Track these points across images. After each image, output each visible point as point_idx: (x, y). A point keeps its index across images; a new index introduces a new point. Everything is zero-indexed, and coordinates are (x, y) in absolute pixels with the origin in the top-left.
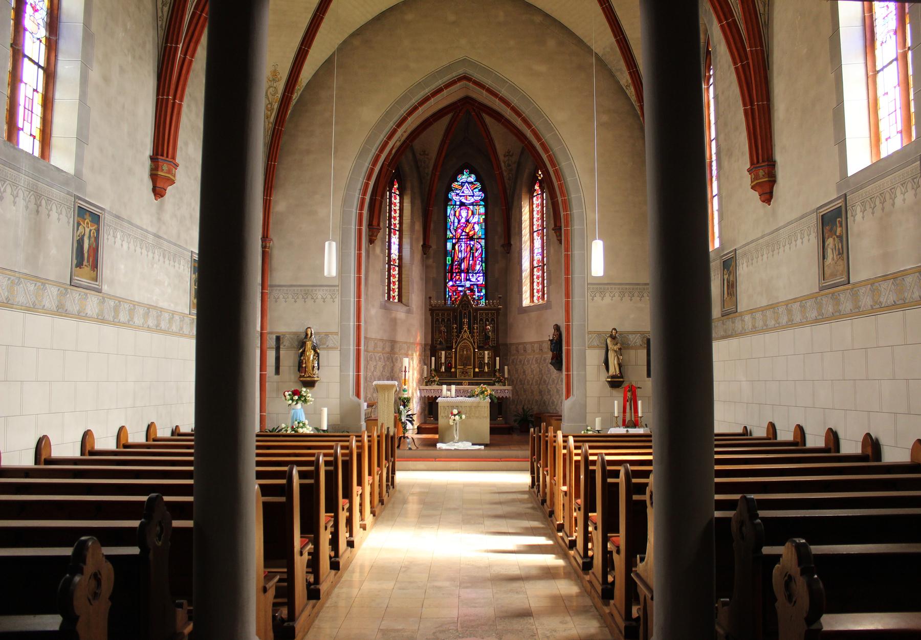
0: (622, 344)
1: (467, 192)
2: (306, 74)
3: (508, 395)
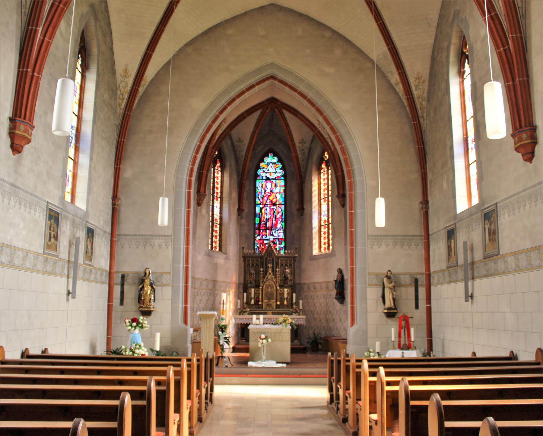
0: (395, 282)
3: (302, 322)
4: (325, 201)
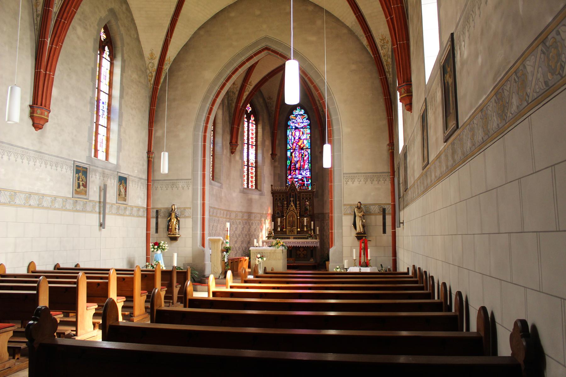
1: (299, 121)
2: (172, 54)
4: (252, 148)
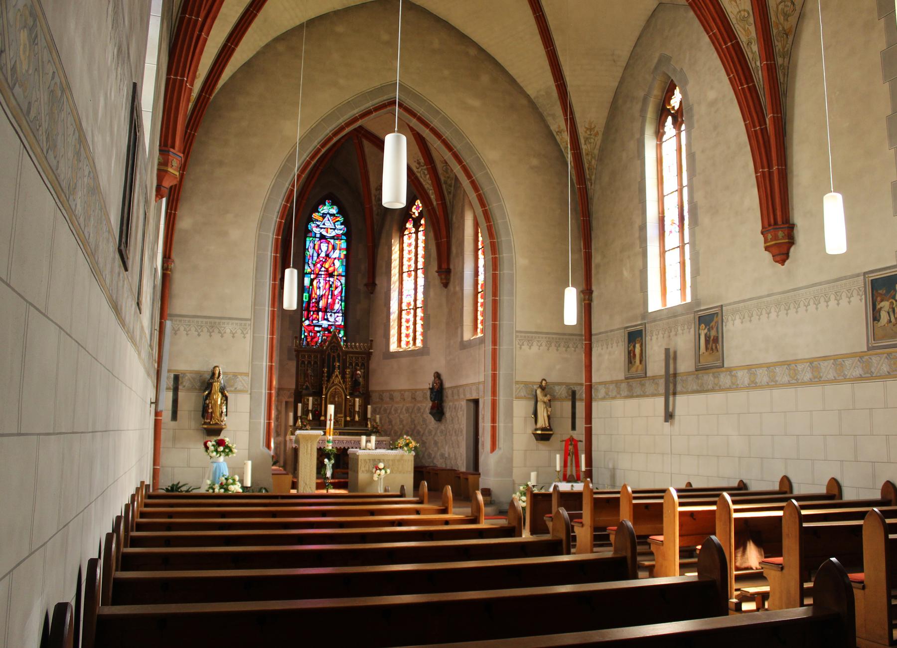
4: (409, 276)
